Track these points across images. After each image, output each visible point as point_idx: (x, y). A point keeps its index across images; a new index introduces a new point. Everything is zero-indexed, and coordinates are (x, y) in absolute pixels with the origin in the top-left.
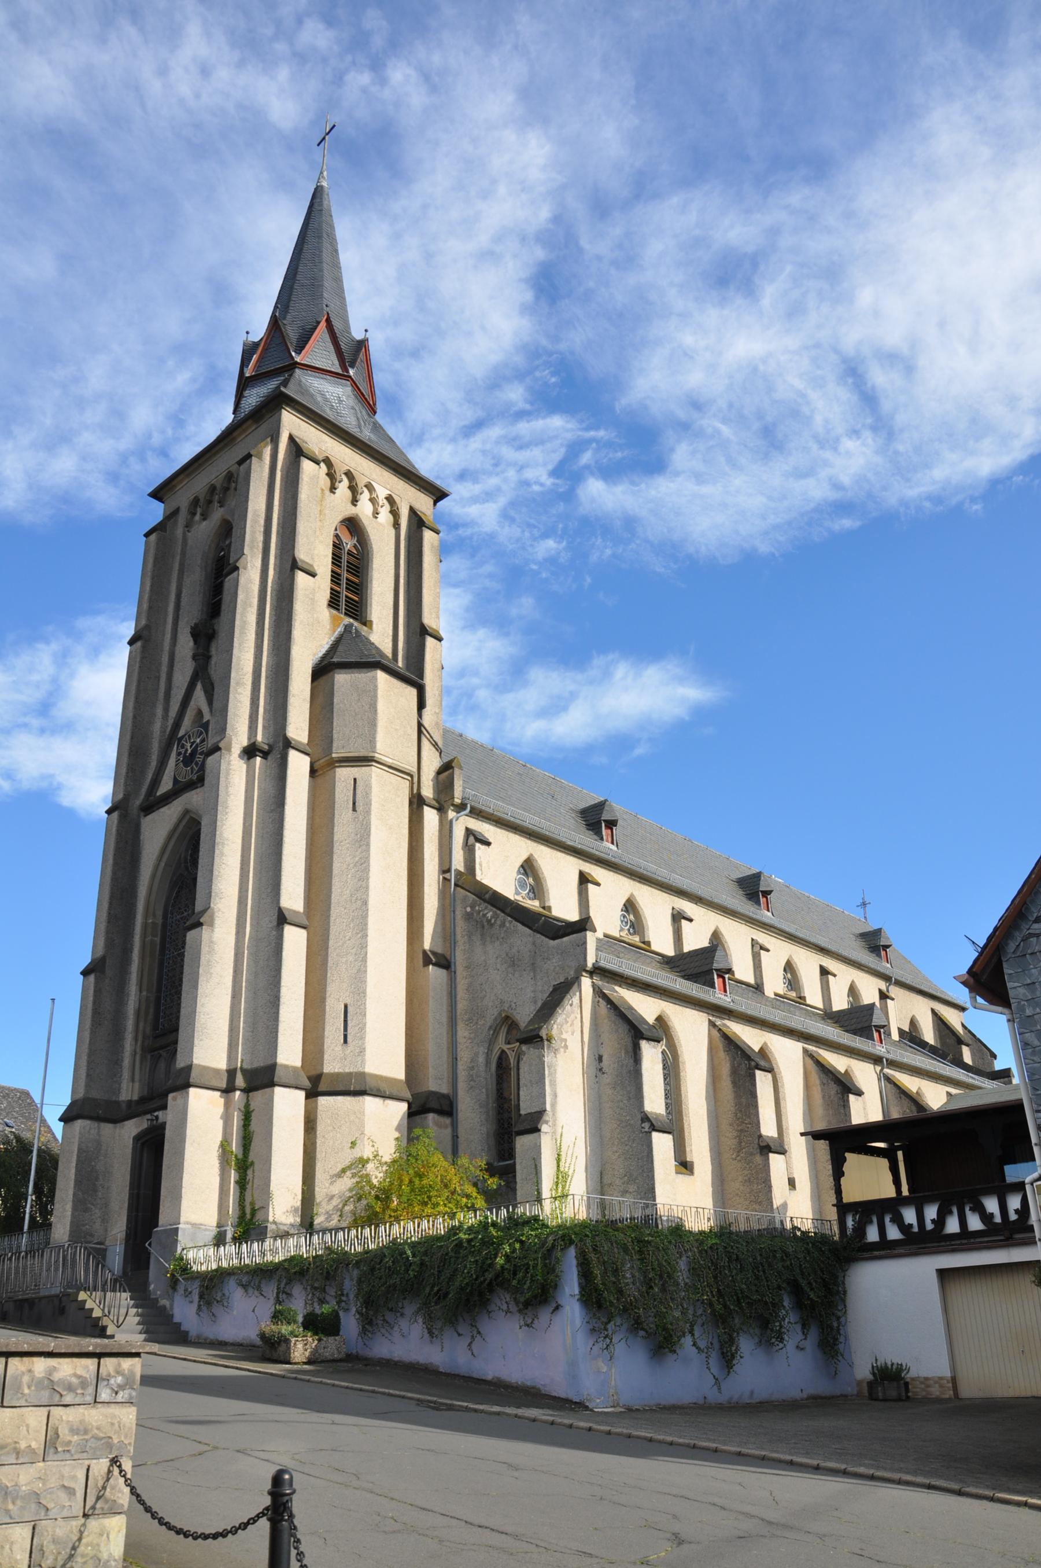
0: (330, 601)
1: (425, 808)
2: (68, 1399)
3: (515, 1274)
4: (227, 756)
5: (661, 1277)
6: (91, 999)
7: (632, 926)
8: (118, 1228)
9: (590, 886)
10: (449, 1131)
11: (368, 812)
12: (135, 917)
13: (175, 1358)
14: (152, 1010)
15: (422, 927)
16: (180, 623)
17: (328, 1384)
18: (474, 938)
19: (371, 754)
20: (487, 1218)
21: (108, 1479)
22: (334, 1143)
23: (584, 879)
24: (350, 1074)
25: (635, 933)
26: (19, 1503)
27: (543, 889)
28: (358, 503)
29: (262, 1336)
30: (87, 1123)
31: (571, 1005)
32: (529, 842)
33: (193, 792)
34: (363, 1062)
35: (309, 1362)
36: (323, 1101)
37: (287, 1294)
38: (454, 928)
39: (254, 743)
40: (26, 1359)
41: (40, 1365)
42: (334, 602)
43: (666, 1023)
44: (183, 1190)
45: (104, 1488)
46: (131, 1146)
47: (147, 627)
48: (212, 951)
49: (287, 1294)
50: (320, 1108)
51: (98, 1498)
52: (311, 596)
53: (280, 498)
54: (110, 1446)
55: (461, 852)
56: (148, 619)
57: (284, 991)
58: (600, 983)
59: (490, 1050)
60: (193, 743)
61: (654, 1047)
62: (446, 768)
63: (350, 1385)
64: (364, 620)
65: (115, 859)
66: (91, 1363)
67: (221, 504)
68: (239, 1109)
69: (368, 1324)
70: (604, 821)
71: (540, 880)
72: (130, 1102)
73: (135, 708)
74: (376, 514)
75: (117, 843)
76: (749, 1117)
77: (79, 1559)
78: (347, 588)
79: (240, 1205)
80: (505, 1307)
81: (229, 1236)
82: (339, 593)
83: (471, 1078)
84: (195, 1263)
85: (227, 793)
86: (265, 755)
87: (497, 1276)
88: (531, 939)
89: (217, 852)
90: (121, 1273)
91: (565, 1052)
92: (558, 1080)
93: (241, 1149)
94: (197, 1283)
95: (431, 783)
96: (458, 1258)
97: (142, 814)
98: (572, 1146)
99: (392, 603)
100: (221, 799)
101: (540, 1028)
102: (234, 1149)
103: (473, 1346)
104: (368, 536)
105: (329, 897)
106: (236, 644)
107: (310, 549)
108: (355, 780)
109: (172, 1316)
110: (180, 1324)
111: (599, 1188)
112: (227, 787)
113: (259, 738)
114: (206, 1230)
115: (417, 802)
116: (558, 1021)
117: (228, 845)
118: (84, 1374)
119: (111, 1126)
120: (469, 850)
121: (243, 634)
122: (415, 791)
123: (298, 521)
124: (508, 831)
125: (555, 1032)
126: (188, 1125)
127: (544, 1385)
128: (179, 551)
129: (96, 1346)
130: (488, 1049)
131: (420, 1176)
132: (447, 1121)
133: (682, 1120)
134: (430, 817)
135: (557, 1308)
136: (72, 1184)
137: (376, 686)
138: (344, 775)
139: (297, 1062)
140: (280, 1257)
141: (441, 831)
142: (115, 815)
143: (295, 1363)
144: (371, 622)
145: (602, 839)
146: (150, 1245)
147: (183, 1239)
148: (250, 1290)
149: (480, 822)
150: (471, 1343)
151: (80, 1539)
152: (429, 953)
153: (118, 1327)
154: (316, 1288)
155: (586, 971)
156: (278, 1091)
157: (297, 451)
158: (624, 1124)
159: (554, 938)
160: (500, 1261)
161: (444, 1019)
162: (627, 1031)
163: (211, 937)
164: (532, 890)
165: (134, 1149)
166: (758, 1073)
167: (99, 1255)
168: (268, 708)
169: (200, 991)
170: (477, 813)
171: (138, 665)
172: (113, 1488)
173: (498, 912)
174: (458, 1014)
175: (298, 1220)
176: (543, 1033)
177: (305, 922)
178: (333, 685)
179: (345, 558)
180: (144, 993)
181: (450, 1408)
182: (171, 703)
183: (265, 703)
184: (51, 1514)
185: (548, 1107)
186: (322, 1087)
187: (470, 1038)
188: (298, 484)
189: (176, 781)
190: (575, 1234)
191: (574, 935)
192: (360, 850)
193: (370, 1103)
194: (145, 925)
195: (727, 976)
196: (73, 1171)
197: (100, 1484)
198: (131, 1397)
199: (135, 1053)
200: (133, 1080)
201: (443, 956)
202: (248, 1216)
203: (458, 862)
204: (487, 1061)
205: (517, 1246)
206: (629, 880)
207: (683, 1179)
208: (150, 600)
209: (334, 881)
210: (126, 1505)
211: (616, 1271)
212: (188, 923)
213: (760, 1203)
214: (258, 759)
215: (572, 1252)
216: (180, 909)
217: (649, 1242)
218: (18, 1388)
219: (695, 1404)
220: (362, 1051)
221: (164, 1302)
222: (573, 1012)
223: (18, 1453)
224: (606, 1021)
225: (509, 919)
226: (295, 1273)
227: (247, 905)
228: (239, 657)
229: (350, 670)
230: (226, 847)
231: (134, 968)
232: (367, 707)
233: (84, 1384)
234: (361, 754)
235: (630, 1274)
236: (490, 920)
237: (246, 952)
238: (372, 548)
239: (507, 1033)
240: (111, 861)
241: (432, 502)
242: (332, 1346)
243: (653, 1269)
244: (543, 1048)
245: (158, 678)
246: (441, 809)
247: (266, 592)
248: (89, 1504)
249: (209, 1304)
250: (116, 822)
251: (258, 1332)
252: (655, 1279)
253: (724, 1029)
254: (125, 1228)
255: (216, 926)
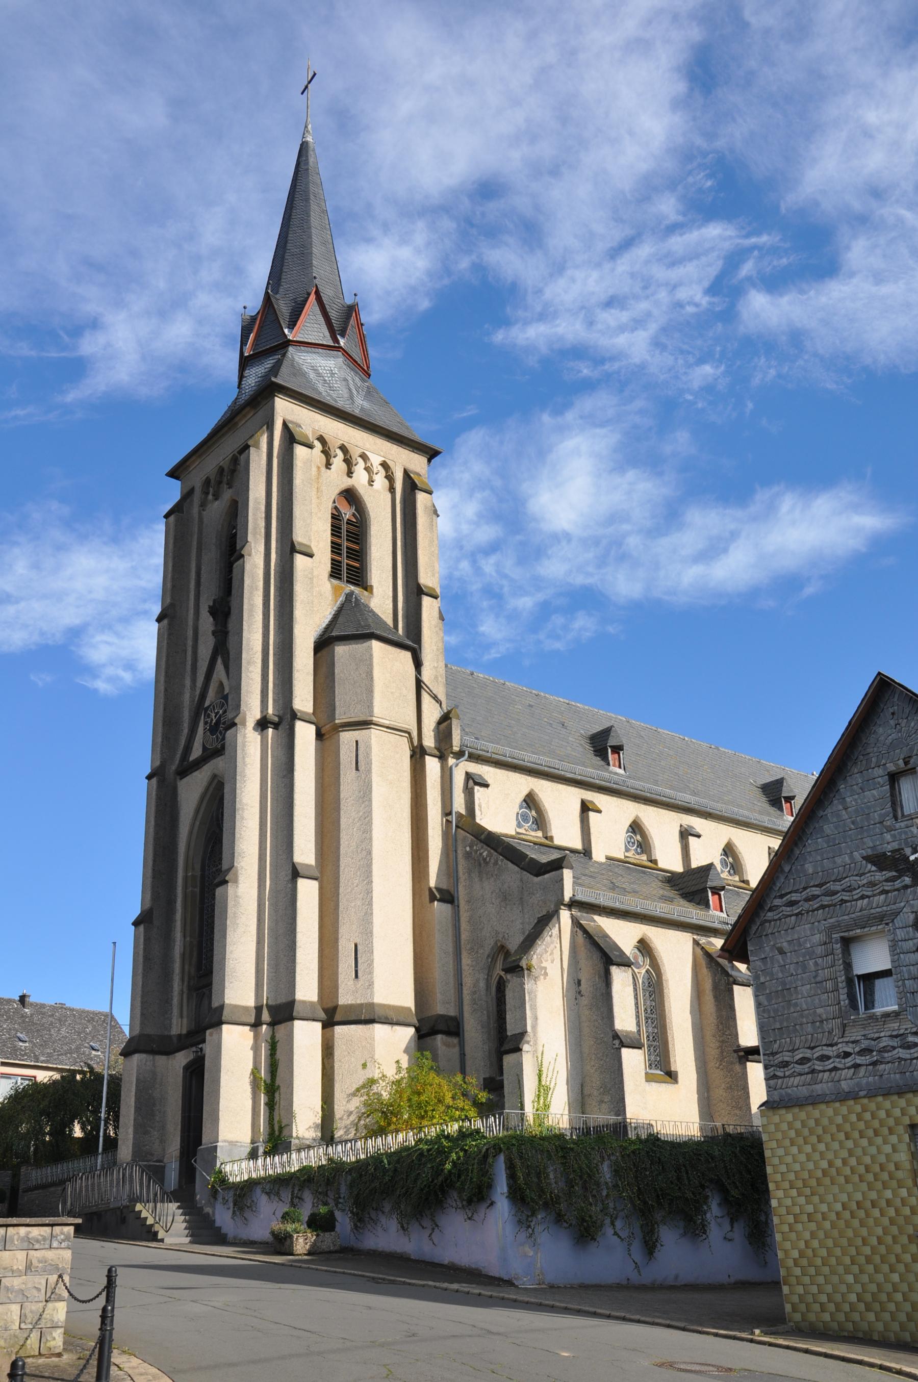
0: (332, 571)
1: (427, 757)
2: (37, 1246)
3: (459, 1177)
4: (243, 731)
5: (581, 1177)
6: (142, 947)
7: (640, 845)
8: (174, 1147)
9: (591, 814)
10: (456, 1050)
11: (369, 771)
12: (177, 871)
13: (206, 1254)
14: (195, 954)
15: (427, 866)
16: (201, 598)
17: (313, 1269)
18: (473, 875)
19: (370, 718)
20: (443, 1131)
21: (57, 1284)
22: (349, 1066)
23: (586, 808)
24: (362, 1004)
25: (642, 852)
26: (14, 1294)
27: (545, 820)
28: (354, 475)
29: (273, 1233)
30: (143, 1056)
31: (551, 936)
32: (529, 778)
33: (219, 758)
34: (372, 994)
35: (309, 1253)
36: (338, 1029)
37: (299, 1198)
38: (457, 865)
39: (266, 716)
40: (16, 1228)
41: (23, 1231)
42: (335, 573)
43: (648, 945)
44: (220, 1113)
45: (55, 1288)
46: (181, 1075)
47: (172, 605)
48: (237, 904)
49: (299, 1198)
50: (336, 1036)
51: (52, 1293)
52: (309, 576)
53: (278, 483)
54: (58, 1269)
55: (462, 795)
56: (172, 598)
57: (299, 937)
58: (579, 914)
59: (489, 975)
60: (217, 714)
61: (625, 971)
62: (445, 718)
63: (329, 1269)
64: (365, 585)
65: (156, 821)
66: (48, 1229)
67: (230, 486)
68: (266, 1041)
69: (360, 1221)
70: (610, 746)
71: (542, 812)
72: (180, 1036)
73: (165, 682)
74: (371, 482)
75: (157, 806)
76: (729, 1029)
77: (43, 1321)
78: (347, 556)
79: (269, 1123)
80: (454, 1205)
81: (261, 1151)
82: (340, 562)
83: (474, 1002)
84: (231, 1175)
85: (244, 763)
86: (276, 726)
87: (446, 1179)
88: (519, 876)
89: (238, 817)
90: (177, 1187)
91: (545, 979)
92: (538, 1005)
93: (269, 1075)
94: (231, 1193)
95: (432, 734)
96: (420, 1164)
97: (178, 777)
98: (553, 1062)
99: (390, 565)
100: (238, 770)
101: (521, 959)
102: (263, 1075)
103: (433, 1236)
104: (365, 504)
105: (338, 848)
106: (245, 627)
107: (307, 531)
108: (357, 742)
109: (214, 1221)
110: (220, 1228)
111: (580, 1099)
112: (244, 758)
113: (270, 710)
114: (241, 1146)
115: (418, 754)
116: (538, 951)
117: (247, 809)
118: (45, 1234)
119: (164, 1057)
120: (469, 792)
121: (251, 615)
122: (416, 744)
123: (294, 507)
124: (508, 770)
125: (534, 961)
126: (223, 1057)
127: (484, 1267)
128: (196, 530)
129: (50, 1221)
130: (488, 975)
131: (419, 1094)
132: (455, 1040)
133: (666, 1033)
134: (432, 765)
135: (492, 1204)
136: (132, 1110)
137: (371, 655)
138: (347, 738)
139: (314, 997)
140: (295, 1168)
141: (442, 777)
142: (154, 780)
143: (298, 1255)
144: (371, 586)
145: (608, 764)
146: (195, 1161)
147: (221, 1155)
148: (272, 1196)
149: (480, 766)
150: (431, 1234)
151: (43, 1312)
152: (434, 890)
153: (167, 1232)
154: (320, 1193)
155: (565, 905)
156: (297, 1024)
157: (291, 438)
158: (599, 1041)
159: (537, 875)
160: (448, 1166)
161: (451, 949)
162: (599, 958)
163: (236, 892)
164: (536, 822)
165: (184, 1077)
166: (736, 988)
167: (157, 1173)
168: (277, 682)
169: (229, 940)
170: (474, 758)
171: (166, 642)
172: (59, 1289)
173: (492, 851)
174: (462, 943)
175: (319, 1134)
176: (523, 963)
177: (317, 874)
178: (334, 656)
179: (344, 527)
180: (188, 939)
181: (393, 1282)
182: (198, 674)
183: (274, 678)
184: (30, 1300)
185: (529, 1029)
186: (337, 1018)
187: (472, 966)
188: (292, 471)
189: (205, 748)
190: (504, 1143)
191: (554, 873)
192: (363, 806)
193: (380, 1030)
194: (186, 878)
195: (722, 893)
196: (133, 1099)
197: (53, 1287)
198: (68, 1245)
199: (182, 991)
200: (181, 1017)
201: (448, 892)
202: (277, 1133)
203: (459, 805)
204: (487, 986)
205: (461, 1154)
206: (634, 803)
207: (663, 1090)
208: (173, 579)
209: (341, 835)
210: (66, 1298)
211: (538, 1175)
212: (216, 881)
213: (740, 1109)
214: (270, 730)
215: (502, 1158)
216: (215, 862)
217: (572, 1149)
218: (12, 1241)
219: (618, 1284)
220: (371, 984)
221: (208, 1210)
222: (552, 943)
223: (13, 1271)
224: (583, 949)
225: (501, 857)
226: (304, 1181)
227: (266, 862)
228: (249, 638)
229: (348, 642)
230: (246, 812)
231: (178, 916)
232: (364, 676)
233: (44, 1239)
234: (361, 719)
235: (554, 1177)
236: (486, 859)
237: (267, 903)
238: (369, 515)
239: (504, 960)
240: (153, 823)
241: (425, 460)
242: (329, 1240)
243: (574, 1171)
244: (523, 977)
245: (185, 651)
246: (442, 757)
247: (269, 575)
248: (48, 1296)
249: (241, 1209)
250: (155, 787)
251: (270, 1231)
252: (575, 1180)
253: (707, 947)
254: (179, 1147)
255: (240, 882)
